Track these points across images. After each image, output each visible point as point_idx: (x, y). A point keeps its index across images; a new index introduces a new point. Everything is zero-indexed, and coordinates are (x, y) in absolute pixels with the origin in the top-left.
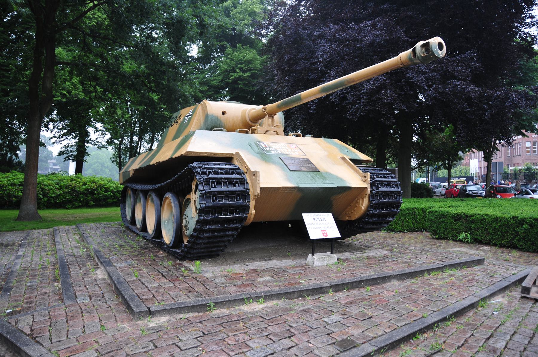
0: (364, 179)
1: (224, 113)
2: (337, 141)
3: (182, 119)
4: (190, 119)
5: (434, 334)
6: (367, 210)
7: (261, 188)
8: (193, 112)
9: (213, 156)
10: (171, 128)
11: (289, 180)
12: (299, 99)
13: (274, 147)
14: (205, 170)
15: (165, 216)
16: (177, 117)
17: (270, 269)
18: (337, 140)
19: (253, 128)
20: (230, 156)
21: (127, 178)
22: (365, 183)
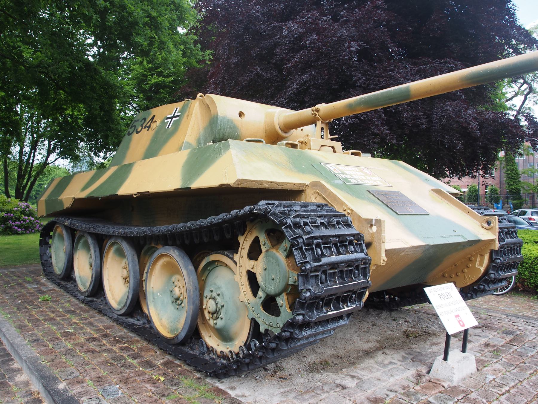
0: (486, 225)
2: (401, 163)
6: (486, 273)
7: (386, 251)
8: (183, 111)
9: (280, 187)
10: (135, 136)
11: (213, 101)
13: (347, 172)
14: (298, 220)
15: (156, 282)
16: (145, 119)
22: (489, 232)
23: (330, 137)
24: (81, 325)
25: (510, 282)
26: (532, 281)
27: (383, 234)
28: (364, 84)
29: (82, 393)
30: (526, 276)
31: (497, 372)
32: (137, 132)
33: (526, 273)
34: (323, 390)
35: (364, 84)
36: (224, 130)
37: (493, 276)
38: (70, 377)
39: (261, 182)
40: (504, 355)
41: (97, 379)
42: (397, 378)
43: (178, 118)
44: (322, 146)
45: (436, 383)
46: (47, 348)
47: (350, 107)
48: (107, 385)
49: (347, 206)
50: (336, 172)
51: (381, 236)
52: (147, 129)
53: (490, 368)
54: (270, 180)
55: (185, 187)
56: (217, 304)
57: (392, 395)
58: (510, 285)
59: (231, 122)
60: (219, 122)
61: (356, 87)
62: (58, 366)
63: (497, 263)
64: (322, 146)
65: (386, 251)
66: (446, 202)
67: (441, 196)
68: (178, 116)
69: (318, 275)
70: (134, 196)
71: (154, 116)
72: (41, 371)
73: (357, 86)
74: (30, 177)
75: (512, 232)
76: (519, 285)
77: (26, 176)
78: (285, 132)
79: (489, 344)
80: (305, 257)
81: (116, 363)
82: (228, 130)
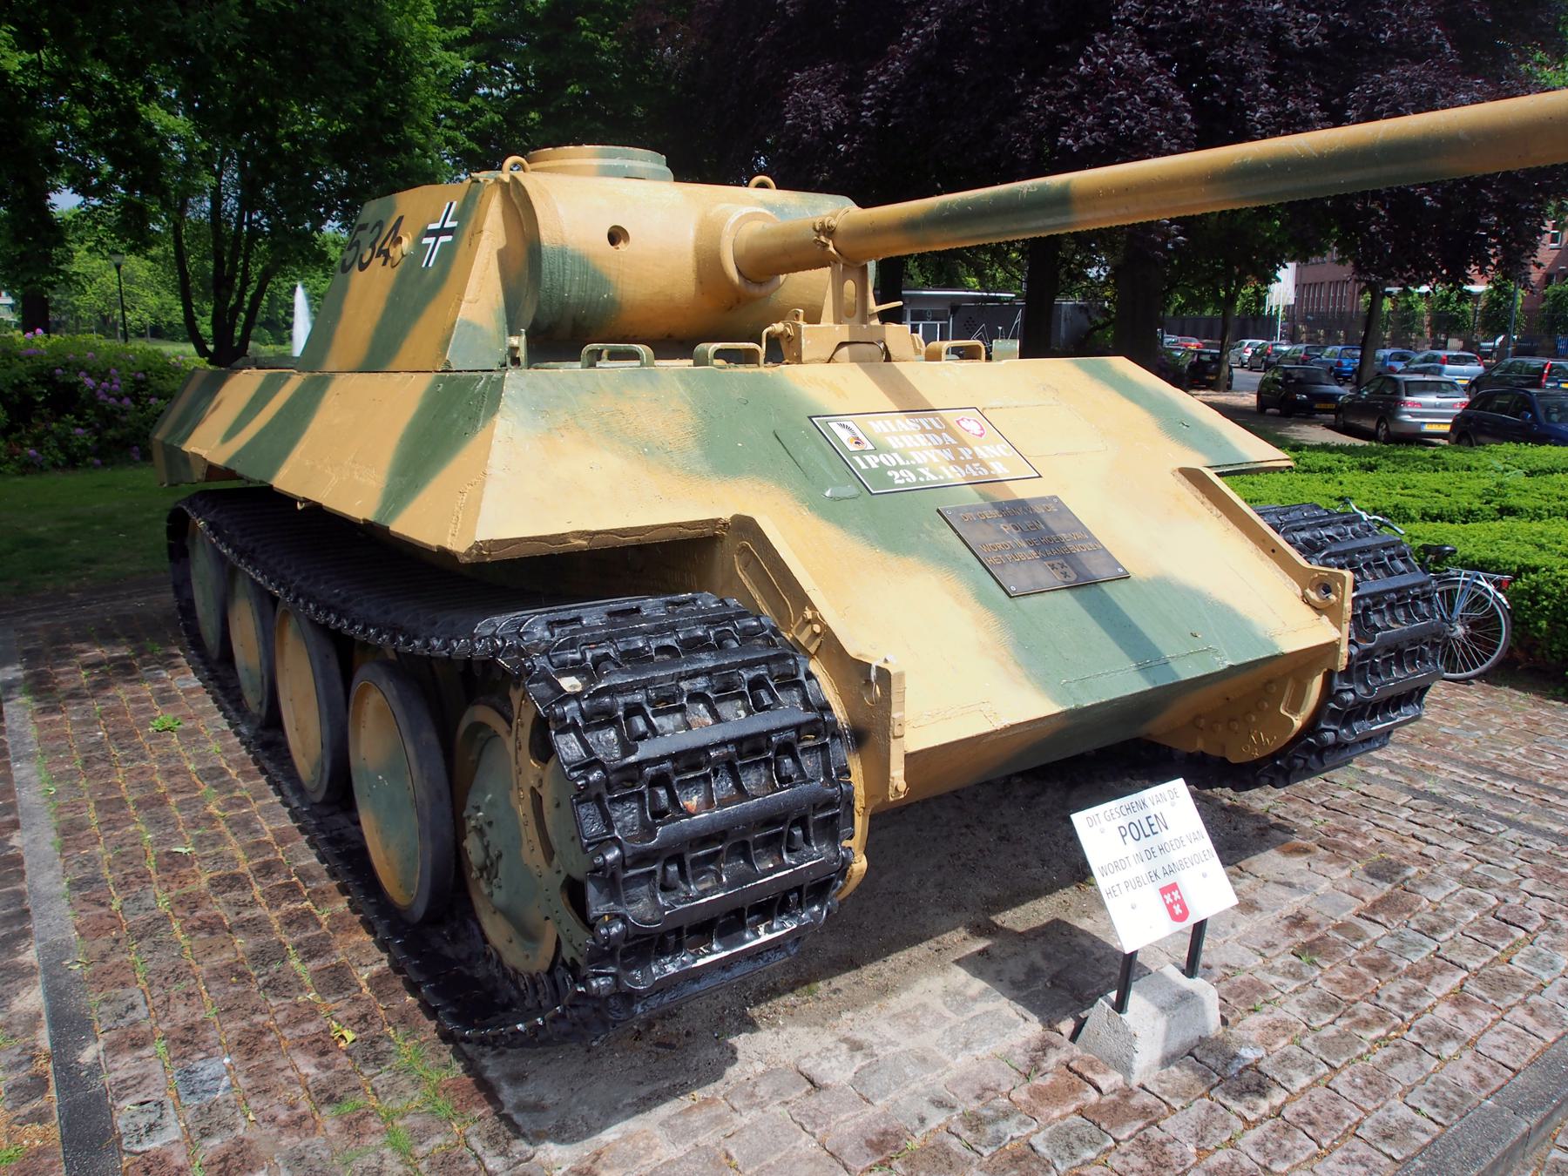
1: (616, 236)
3: (406, 244)
4: (448, 253)
5: (529, 21)
6: (1311, 727)
7: (909, 757)
9: (631, 540)
12: (1062, 200)
13: (894, 442)
16: (380, 224)
17: (929, 1029)
18: (1122, 359)
19: (778, 327)
20: (707, 531)
21: (254, 474)
23: (873, 307)
24: (223, 827)
25: (1488, 643)
26: (1556, 647)
27: (895, 715)
28: (1139, 14)
29: (130, 1083)
30: (1539, 630)
31: (1280, 1031)
32: (363, 267)
33: (1543, 624)
34: (752, 1095)
35: (1139, 14)
36: (563, 289)
37: (1329, 736)
38: (121, 1023)
39: (562, 538)
40: (1327, 966)
41: (182, 1035)
42: (979, 1053)
43: (449, 238)
44: (842, 344)
45: (1081, 1076)
46: (103, 910)
47: (910, 226)
48: (202, 1055)
49: (813, 607)
50: (852, 447)
51: (889, 718)
52: (382, 259)
53: (1264, 1017)
54: (593, 528)
55: (382, 522)
56: (486, 848)
57: (937, 1118)
58: (1493, 653)
59: (582, 262)
60: (545, 265)
61: (1112, 22)
62: (107, 979)
63: (1344, 703)
64: (842, 344)
65: (909, 757)
66: (1216, 511)
67: (1202, 491)
68: (450, 231)
69: (653, 872)
70: (299, 506)
71: (401, 218)
72: (62, 994)
73: (1118, 21)
74: (246, 281)
75: (1416, 597)
76: (1518, 654)
77: (237, 280)
78: (760, 283)
79: (1304, 918)
80: (609, 823)
81: (255, 973)
82: (575, 289)
